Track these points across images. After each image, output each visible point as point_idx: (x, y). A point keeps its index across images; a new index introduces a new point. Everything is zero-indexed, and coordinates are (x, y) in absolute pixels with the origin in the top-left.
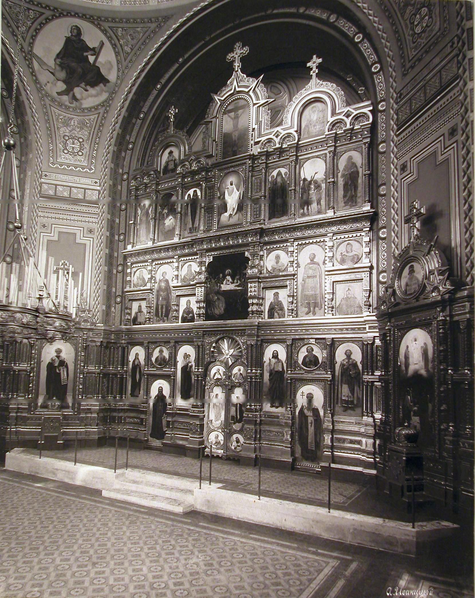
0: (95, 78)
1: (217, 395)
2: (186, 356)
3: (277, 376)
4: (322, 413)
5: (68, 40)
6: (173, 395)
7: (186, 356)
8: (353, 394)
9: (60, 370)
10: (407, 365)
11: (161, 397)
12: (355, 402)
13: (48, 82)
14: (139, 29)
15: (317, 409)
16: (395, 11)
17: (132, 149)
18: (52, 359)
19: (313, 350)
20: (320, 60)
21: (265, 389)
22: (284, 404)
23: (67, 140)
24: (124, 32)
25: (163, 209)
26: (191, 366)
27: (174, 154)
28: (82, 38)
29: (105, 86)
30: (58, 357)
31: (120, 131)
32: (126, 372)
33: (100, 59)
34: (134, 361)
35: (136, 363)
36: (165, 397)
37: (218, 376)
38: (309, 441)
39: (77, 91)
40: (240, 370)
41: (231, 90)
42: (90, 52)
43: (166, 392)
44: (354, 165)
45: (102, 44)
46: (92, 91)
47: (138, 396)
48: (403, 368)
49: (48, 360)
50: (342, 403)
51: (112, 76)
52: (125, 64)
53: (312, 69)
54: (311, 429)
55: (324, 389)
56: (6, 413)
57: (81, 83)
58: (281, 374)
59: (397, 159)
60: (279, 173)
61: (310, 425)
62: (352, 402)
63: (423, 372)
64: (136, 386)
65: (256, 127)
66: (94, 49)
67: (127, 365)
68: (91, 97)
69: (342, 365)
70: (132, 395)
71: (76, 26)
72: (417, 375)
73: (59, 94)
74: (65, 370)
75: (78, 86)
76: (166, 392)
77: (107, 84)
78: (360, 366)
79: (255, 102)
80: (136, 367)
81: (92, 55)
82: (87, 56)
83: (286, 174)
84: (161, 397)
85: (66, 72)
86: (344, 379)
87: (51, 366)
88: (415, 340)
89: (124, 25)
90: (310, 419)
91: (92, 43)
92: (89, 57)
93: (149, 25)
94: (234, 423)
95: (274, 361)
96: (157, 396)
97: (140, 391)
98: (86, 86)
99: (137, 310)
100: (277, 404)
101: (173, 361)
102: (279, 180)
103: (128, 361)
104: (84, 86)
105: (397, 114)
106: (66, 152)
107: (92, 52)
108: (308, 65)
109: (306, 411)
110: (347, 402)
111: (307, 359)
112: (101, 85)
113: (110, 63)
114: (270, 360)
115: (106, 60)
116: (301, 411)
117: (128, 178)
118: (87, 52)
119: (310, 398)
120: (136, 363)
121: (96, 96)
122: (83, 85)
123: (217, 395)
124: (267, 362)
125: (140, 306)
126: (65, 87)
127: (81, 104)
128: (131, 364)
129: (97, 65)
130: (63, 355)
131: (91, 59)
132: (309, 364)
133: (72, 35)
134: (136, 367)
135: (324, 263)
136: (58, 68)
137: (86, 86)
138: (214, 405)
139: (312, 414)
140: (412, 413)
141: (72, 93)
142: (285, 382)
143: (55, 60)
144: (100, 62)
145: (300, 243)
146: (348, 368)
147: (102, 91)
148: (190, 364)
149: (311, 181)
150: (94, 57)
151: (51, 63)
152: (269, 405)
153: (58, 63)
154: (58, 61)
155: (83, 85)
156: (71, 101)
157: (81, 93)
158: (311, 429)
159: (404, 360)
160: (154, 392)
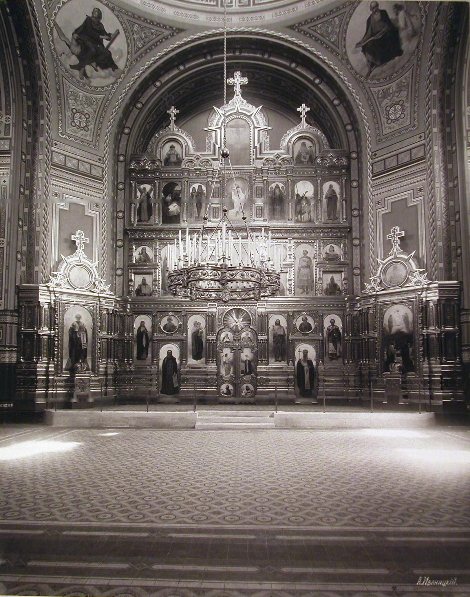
0: (106, 62)
1: (226, 355)
2: (196, 324)
3: (280, 339)
4: (314, 363)
5: (88, 19)
6: (183, 355)
7: (196, 324)
8: (336, 349)
9: (80, 335)
10: (390, 327)
11: (170, 357)
12: (338, 355)
13: (64, 53)
14: (153, 31)
15: (311, 361)
16: (374, 98)
17: (129, 134)
18: (73, 325)
19: (307, 319)
20: (309, 109)
21: (271, 349)
22: (286, 358)
23: (75, 114)
24: (139, 29)
25: (166, 195)
26: (202, 333)
27: (176, 149)
28: (101, 21)
29: (113, 71)
30: (78, 322)
31: (122, 115)
32: (132, 337)
33: (112, 46)
34: (139, 328)
35: (142, 330)
36: (174, 359)
37: (226, 340)
38: (306, 383)
39: (89, 69)
40: (248, 334)
41: (234, 109)
42: (105, 37)
43: (176, 354)
44: (334, 192)
45: (118, 33)
46: (102, 73)
47: (145, 359)
48: (387, 328)
49: (70, 326)
50: (328, 355)
51: (121, 64)
52: (135, 56)
53: (301, 114)
54: (307, 375)
55: (316, 348)
56: (33, 377)
57: (93, 62)
58: (282, 336)
59: (373, 196)
60: (277, 187)
61: (306, 372)
62: (336, 354)
63: (405, 330)
64: (142, 352)
65: (258, 146)
66: (109, 35)
67: (133, 332)
68: (99, 78)
69: (328, 329)
70: (139, 358)
71: (99, 9)
72: (399, 333)
73: (72, 67)
74: (85, 335)
75: (90, 64)
76: (176, 354)
77: (116, 70)
78: (341, 331)
79: (256, 125)
80: (142, 333)
81: (106, 39)
82: (102, 39)
83: (282, 187)
84: (170, 357)
85: (81, 48)
86: (330, 338)
87: (72, 330)
88: (398, 311)
89: (142, 23)
90: (306, 368)
91: (109, 29)
92: (104, 40)
93: (163, 30)
94: (244, 376)
95: (277, 327)
96: (167, 358)
97: (147, 354)
98: (97, 66)
99: (140, 283)
100: (280, 359)
101: (183, 328)
102: (277, 191)
103: (133, 328)
104: (95, 66)
105: (372, 166)
106: (73, 124)
107: (108, 37)
108: (298, 109)
109: (302, 363)
110: (332, 355)
111: (303, 326)
112: (110, 69)
113: (121, 51)
114: (273, 326)
115: (118, 48)
116: (299, 363)
117: (125, 160)
118: (103, 35)
119: (305, 353)
120: (142, 330)
121: (105, 78)
122: (94, 64)
123: (226, 355)
124: (271, 328)
125: (144, 280)
126: (78, 62)
127: (90, 82)
128: (135, 332)
129: (109, 49)
130: (82, 321)
131: (106, 43)
132: (305, 330)
133: (93, 16)
134: (142, 333)
135: (314, 258)
136: (74, 42)
137: (97, 66)
138: (225, 363)
139: (307, 365)
140: (395, 355)
141: (83, 69)
142: (286, 343)
143: (73, 34)
144: (113, 49)
145: (296, 241)
146: (332, 332)
147: (110, 75)
148: (200, 331)
149: (303, 197)
150: (108, 42)
151: (69, 36)
152: (274, 360)
153: (75, 38)
154: (76, 36)
155: (94, 64)
156: (82, 77)
157: (92, 72)
158: (307, 375)
159: (387, 323)
160: (163, 354)
